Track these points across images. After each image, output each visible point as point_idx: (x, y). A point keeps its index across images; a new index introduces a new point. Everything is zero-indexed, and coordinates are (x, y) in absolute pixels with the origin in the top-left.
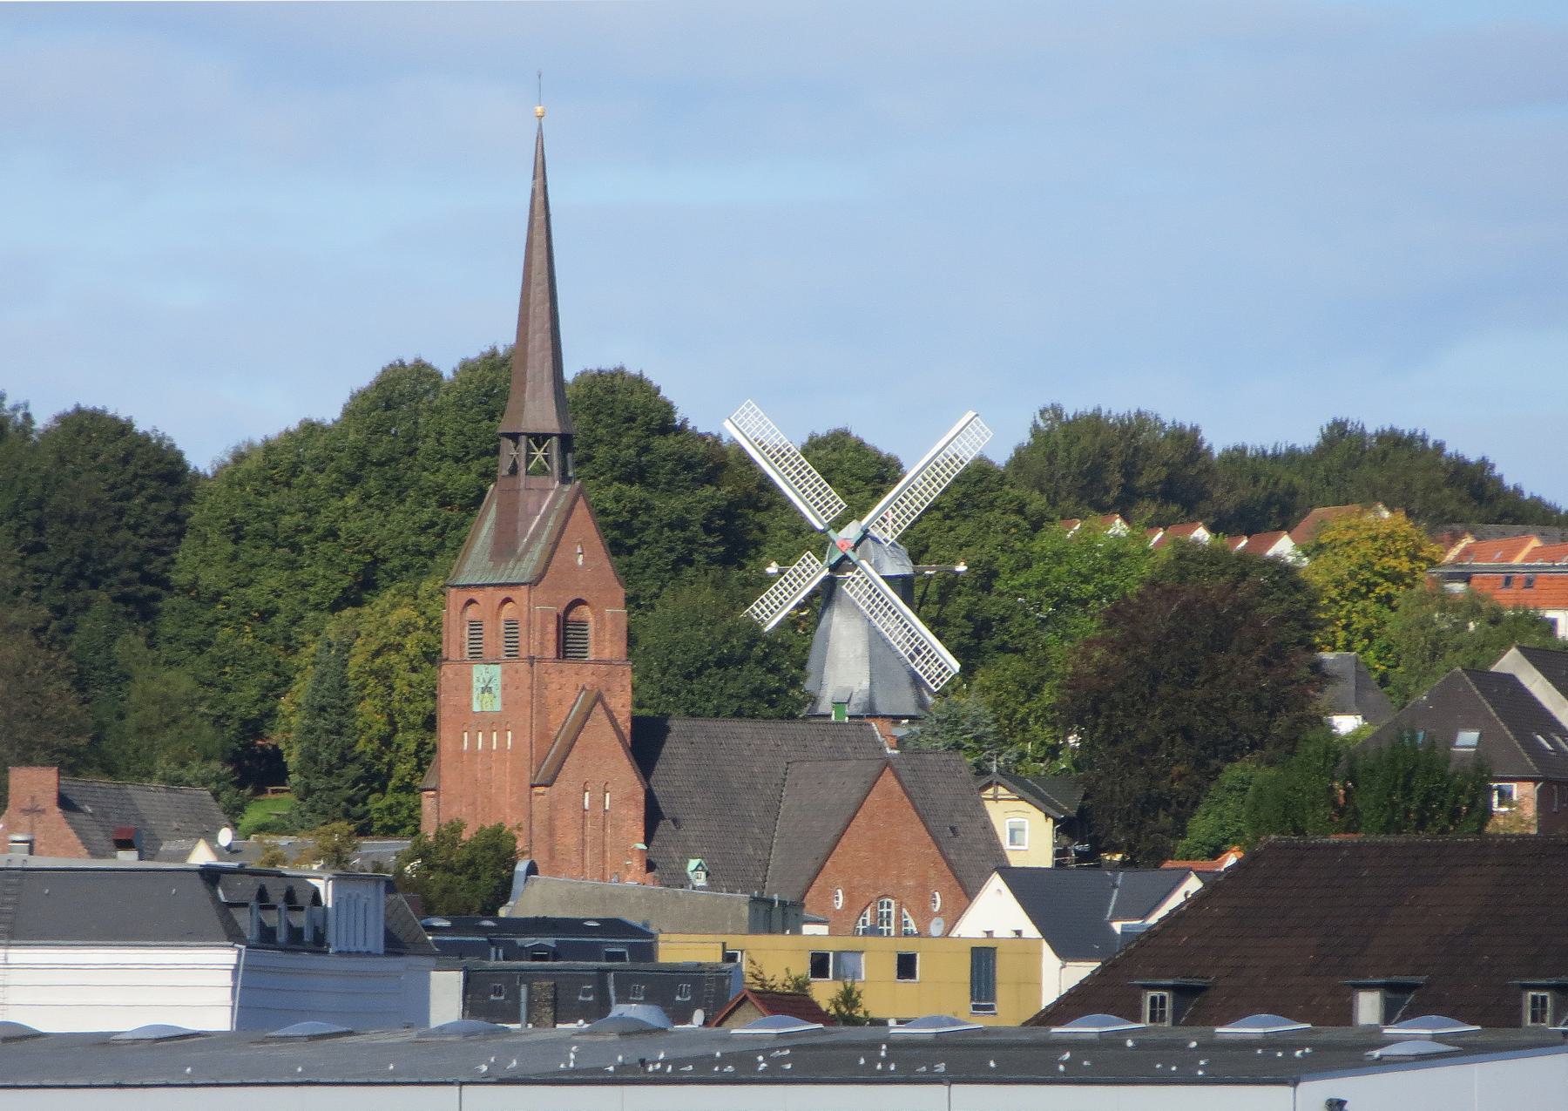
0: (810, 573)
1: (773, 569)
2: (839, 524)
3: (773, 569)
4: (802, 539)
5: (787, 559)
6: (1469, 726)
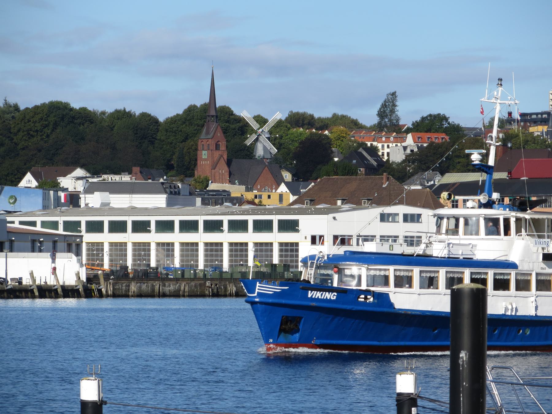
0: (254, 137)
1: (248, 136)
2: (259, 129)
3: (248, 136)
4: (253, 131)
5: (251, 134)
6: (355, 160)
